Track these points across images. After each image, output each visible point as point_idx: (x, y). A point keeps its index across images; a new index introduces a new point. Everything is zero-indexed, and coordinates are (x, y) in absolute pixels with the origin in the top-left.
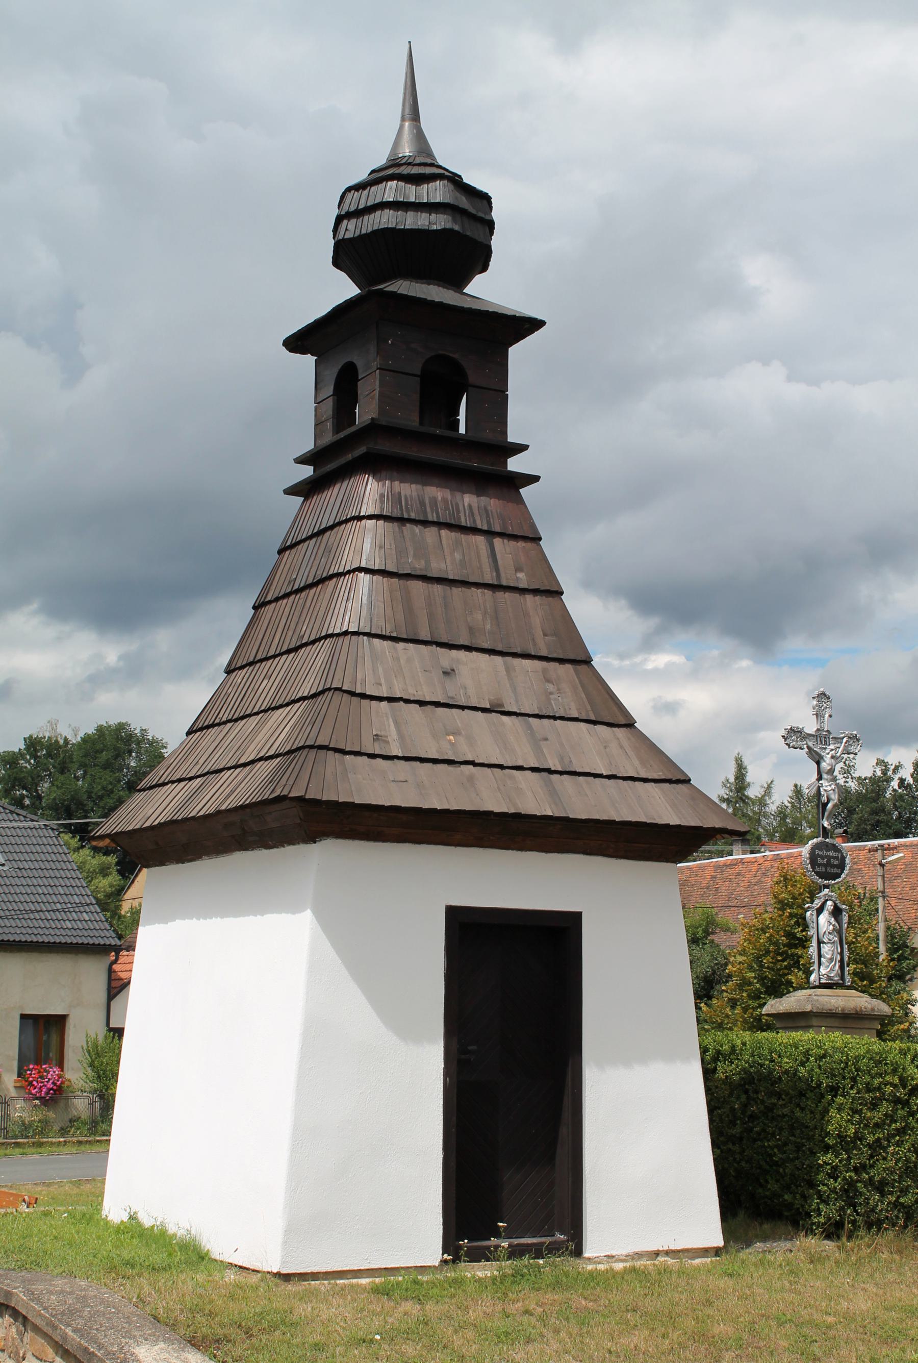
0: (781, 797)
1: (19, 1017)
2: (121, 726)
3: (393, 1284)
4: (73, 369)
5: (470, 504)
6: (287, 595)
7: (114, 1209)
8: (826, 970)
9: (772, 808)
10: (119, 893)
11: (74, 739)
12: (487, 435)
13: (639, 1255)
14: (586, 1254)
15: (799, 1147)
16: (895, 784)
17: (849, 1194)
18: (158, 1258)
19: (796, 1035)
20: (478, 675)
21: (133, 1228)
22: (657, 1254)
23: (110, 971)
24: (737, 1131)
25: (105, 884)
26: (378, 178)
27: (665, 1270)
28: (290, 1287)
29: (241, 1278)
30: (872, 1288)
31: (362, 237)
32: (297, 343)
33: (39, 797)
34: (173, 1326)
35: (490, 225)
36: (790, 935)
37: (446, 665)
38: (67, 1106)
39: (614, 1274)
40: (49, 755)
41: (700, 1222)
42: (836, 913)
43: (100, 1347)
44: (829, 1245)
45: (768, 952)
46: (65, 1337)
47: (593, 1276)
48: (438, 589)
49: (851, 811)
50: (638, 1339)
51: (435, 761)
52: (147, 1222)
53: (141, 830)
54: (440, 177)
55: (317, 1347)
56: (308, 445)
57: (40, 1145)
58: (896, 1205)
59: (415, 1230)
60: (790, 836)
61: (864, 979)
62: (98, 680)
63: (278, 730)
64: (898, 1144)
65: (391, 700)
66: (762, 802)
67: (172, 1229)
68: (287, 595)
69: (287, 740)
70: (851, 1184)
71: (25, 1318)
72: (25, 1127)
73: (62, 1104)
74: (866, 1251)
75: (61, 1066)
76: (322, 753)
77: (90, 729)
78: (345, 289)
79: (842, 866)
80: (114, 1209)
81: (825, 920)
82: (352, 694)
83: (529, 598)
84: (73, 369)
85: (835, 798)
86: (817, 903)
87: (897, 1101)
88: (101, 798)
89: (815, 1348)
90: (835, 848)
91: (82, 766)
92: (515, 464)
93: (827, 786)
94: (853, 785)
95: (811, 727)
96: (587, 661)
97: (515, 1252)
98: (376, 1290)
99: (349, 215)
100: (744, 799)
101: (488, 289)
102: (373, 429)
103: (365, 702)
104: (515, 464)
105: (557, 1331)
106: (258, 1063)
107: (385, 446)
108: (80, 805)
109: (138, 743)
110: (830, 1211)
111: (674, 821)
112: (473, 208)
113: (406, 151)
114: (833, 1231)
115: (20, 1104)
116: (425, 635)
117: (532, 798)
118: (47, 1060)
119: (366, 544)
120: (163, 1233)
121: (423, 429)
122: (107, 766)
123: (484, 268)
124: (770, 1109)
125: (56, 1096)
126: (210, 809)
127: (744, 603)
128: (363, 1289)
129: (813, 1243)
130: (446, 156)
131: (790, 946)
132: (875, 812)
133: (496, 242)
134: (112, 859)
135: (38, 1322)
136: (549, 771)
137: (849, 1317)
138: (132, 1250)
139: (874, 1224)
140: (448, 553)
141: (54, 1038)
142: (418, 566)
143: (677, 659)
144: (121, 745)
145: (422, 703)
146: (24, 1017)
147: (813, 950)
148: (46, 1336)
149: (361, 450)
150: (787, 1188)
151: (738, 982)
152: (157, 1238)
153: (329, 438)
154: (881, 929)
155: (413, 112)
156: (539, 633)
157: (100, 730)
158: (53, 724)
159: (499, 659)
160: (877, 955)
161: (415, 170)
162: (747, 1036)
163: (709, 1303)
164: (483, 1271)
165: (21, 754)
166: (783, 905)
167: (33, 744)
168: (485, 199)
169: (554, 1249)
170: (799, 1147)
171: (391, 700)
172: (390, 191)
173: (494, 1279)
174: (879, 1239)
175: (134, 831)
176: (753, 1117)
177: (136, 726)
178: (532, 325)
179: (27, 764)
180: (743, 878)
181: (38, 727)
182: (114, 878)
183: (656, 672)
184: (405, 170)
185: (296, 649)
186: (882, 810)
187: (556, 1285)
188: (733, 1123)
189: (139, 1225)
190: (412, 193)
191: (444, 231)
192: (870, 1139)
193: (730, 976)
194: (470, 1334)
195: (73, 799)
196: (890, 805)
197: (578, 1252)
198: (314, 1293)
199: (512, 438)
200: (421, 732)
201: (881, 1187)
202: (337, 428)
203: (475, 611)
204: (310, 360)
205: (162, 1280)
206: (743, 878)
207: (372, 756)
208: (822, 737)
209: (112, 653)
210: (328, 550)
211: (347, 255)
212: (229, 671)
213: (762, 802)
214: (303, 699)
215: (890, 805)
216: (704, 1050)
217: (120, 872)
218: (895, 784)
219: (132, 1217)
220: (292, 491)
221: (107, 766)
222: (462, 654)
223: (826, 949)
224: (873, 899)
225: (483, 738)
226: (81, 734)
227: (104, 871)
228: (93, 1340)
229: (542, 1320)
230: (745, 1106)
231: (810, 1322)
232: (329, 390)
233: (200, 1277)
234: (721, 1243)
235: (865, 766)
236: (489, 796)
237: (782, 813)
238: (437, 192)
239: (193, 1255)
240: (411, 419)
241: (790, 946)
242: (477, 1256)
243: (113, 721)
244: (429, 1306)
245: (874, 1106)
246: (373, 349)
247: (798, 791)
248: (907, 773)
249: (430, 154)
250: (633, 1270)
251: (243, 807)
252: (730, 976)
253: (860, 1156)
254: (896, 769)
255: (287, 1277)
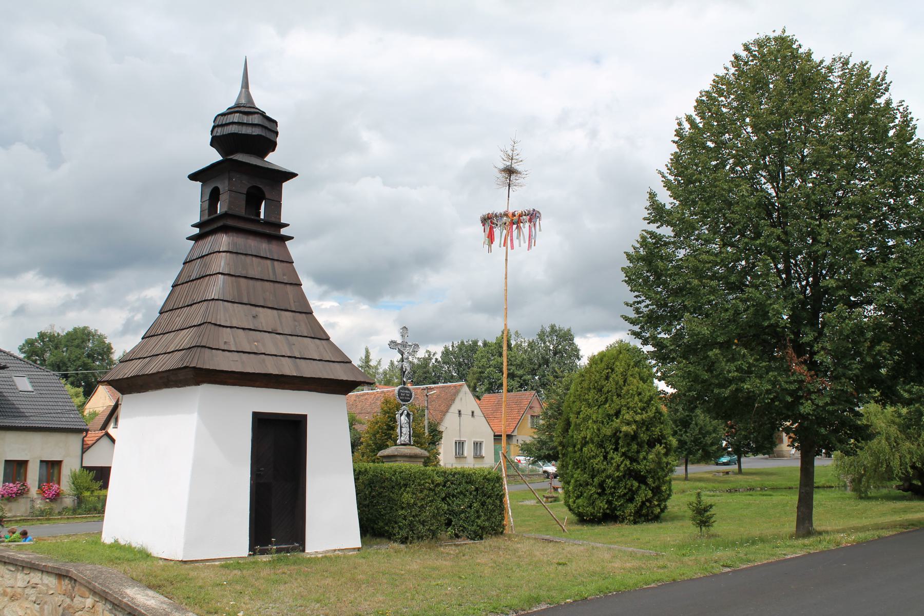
0: (385, 366)
1: (38, 464)
2: (85, 328)
3: (228, 564)
4: (56, 162)
5: (263, 247)
6: (187, 282)
7: (107, 538)
8: (404, 438)
9: (381, 371)
10: (84, 404)
11: (63, 334)
12: (273, 219)
13: (328, 551)
14: (307, 551)
15: (391, 508)
16: (433, 361)
17: (411, 526)
18: (130, 556)
19: (391, 464)
20: (267, 318)
21: (116, 545)
22: (335, 550)
23: (83, 441)
24: (367, 502)
25: (78, 401)
26: (230, 112)
27: (338, 557)
28: (187, 566)
29: (165, 563)
30: (418, 561)
31: (223, 136)
32: (194, 177)
33: (45, 360)
34: (140, 581)
35: (277, 133)
36: (388, 425)
37: (254, 313)
38: (61, 502)
39: (318, 559)
40: (50, 341)
41: (352, 538)
42: (408, 415)
43: (111, 590)
44: (402, 546)
45: (378, 432)
46: (95, 587)
47: (310, 559)
48: (251, 282)
49: (415, 372)
50: (329, 581)
51: (249, 353)
52: (122, 542)
53: (122, 379)
54: (257, 113)
55: (201, 587)
56: (197, 220)
57: (49, 519)
58: (429, 530)
59: (237, 542)
60: (388, 383)
61: (418, 443)
62: (66, 306)
63: (185, 339)
64: (431, 506)
65: (231, 327)
66: (376, 368)
67: (134, 545)
68: (187, 282)
69: (187, 344)
70: (412, 522)
71: (75, 580)
72: (42, 513)
73: (59, 501)
74: (417, 548)
75: (59, 483)
76: (203, 349)
77: (70, 329)
78: (215, 156)
79: (411, 397)
80: (107, 538)
81: (404, 418)
82: (215, 325)
83: (288, 286)
84: (56, 162)
85: (408, 369)
86: (401, 412)
87: (430, 489)
88: (74, 361)
89: (397, 582)
90: (408, 389)
91: (66, 346)
92: (284, 232)
93: (406, 364)
94: (416, 361)
95: (399, 341)
96: (311, 313)
97: (279, 551)
98: (222, 566)
99: (218, 126)
100: (369, 366)
101: (274, 159)
102: (225, 215)
103: (221, 328)
104: (284, 232)
105: (296, 579)
106: (172, 477)
107: (230, 222)
108: (64, 364)
109: (93, 336)
110: (404, 533)
111: (345, 378)
112: (270, 125)
113: (243, 101)
114: (404, 541)
115: (39, 501)
116: (245, 301)
117: (288, 368)
118: (52, 481)
119: (221, 263)
120: (130, 547)
121: (247, 216)
122: (78, 346)
123: (273, 150)
124: (380, 493)
125: (56, 497)
126: (154, 371)
127: (370, 281)
128: (217, 566)
129: (396, 545)
130: (260, 104)
131: (388, 429)
132: (425, 373)
133: (279, 140)
134: (81, 389)
135: (82, 581)
136: (295, 358)
137: (409, 571)
138: (117, 553)
139: (420, 538)
140: (255, 268)
141: (56, 471)
142: (244, 273)
143: (336, 304)
144: (85, 337)
145: (243, 329)
146: (41, 461)
147: (398, 430)
148: (86, 586)
149: (220, 224)
150: (387, 524)
151: (371, 443)
152: (128, 549)
153: (206, 217)
154: (426, 423)
155: (245, 85)
156: (292, 301)
157: (75, 329)
158: (52, 326)
159: (275, 311)
160: (424, 433)
161: (247, 110)
162: (371, 464)
163: (356, 568)
164: (265, 558)
165: (36, 340)
166: (385, 412)
167: (42, 336)
168: (275, 122)
169: (294, 549)
170: (391, 508)
171: (231, 327)
172: (236, 118)
173: (270, 561)
174: (422, 543)
175: (119, 380)
176: (373, 497)
177: (92, 328)
178: (293, 175)
179: (39, 345)
180: (368, 400)
181: (44, 327)
182: (82, 398)
183: (326, 309)
184: (242, 109)
185: (191, 305)
186: (428, 372)
187: (295, 563)
188: (365, 499)
189: (119, 544)
190: (245, 119)
191: (258, 135)
192: (419, 504)
193: (362, 443)
194: (262, 581)
195: (61, 361)
196: (431, 370)
197: (304, 550)
198: (197, 568)
199: (283, 221)
200: (243, 341)
201: (423, 523)
202: (209, 215)
203: (264, 292)
204: (199, 184)
205: (133, 564)
206: (368, 400)
207: (224, 350)
208: (404, 345)
209: (74, 292)
210: (205, 265)
211: (216, 142)
212: (161, 313)
213: (376, 368)
214: (195, 326)
215: (431, 370)
216: (354, 470)
217: (84, 395)
218: (433, 361)
219: (116, 541)
220: (189, 238)
221: (78, 346)
222: (260, 309)
223: (404, 430)
224: (423, 411)
225: (269, 344)
226: (66, 332)
227: (77, 395)
228: (108, 587)
229: (290, 575)
230: (370, 493)
231: (395, 574)
232: (207, 197)
233: (149, 563)
234: (360, 546)
235: (421, 353)
236: (271, 367)
237: (385, 373)
238: (256, 119)
239: (144, 555)
240: (241, 211)
241: (388, 429)
242: (263, 552)
243: (81, 326)
244: (245, 572)
245: (421, 492)
246: (227, 182)
247: (392, 363)
248: (439, 356)
249: (253, 103)
250: (326, 557)
251: (169, 370)
252: (362, 443)
253: (416, 510)
254: (434, 354)
255: (185, 562)
